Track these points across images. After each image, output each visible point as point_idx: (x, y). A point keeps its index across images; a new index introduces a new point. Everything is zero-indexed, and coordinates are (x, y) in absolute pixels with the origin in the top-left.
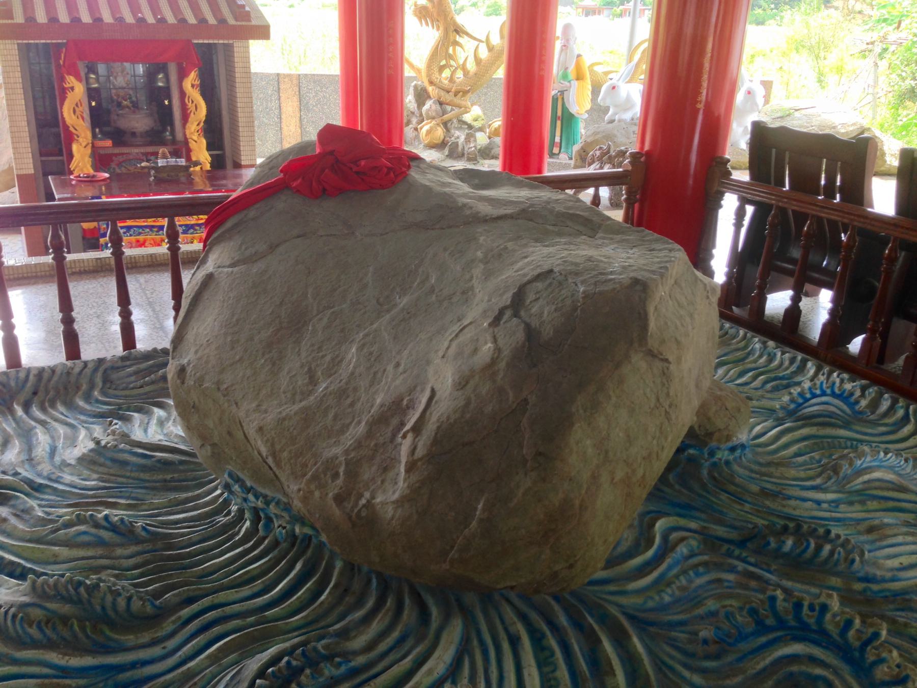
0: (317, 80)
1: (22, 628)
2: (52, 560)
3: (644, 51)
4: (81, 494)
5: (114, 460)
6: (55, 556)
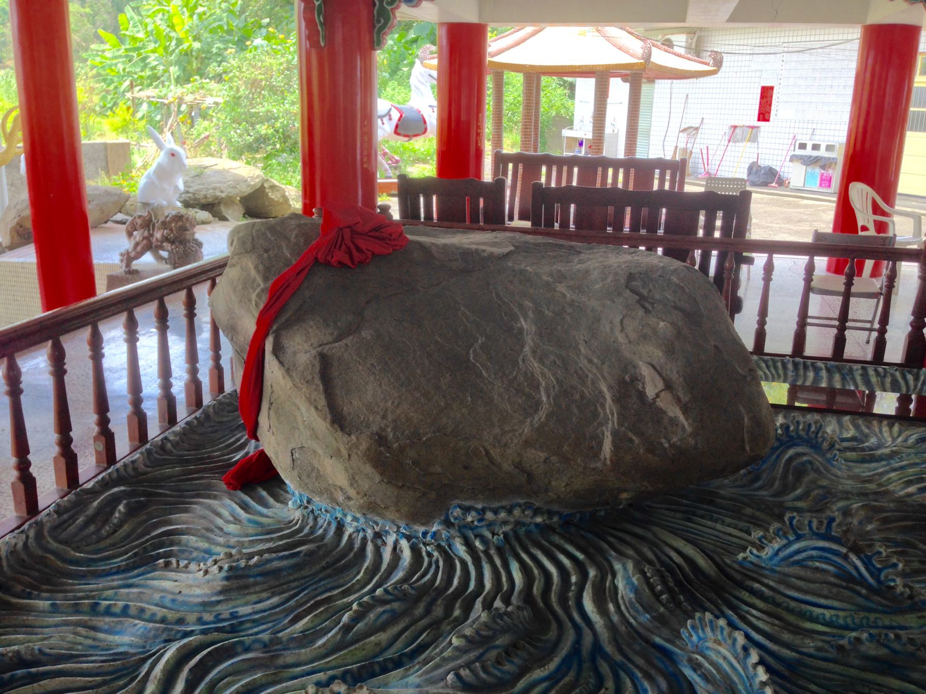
0: (911, 130)
1: (498, 670)
2: (378, 649)
3: (15, 120)
4: (284, 610)
5: (262, 574)
6: (378, 644)
